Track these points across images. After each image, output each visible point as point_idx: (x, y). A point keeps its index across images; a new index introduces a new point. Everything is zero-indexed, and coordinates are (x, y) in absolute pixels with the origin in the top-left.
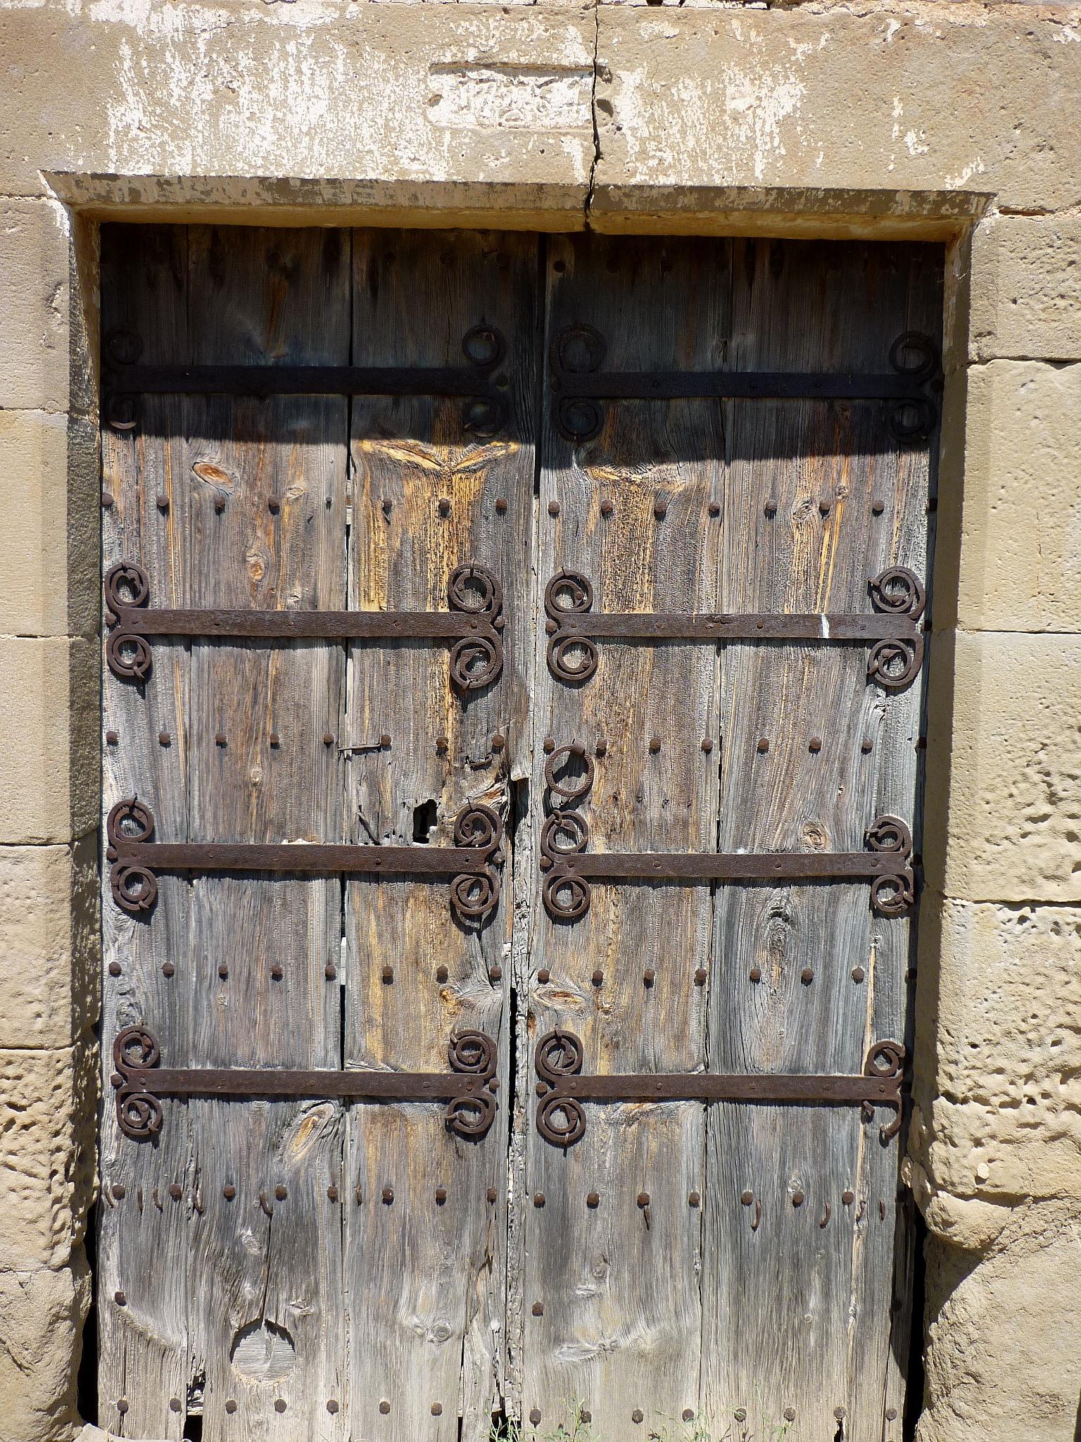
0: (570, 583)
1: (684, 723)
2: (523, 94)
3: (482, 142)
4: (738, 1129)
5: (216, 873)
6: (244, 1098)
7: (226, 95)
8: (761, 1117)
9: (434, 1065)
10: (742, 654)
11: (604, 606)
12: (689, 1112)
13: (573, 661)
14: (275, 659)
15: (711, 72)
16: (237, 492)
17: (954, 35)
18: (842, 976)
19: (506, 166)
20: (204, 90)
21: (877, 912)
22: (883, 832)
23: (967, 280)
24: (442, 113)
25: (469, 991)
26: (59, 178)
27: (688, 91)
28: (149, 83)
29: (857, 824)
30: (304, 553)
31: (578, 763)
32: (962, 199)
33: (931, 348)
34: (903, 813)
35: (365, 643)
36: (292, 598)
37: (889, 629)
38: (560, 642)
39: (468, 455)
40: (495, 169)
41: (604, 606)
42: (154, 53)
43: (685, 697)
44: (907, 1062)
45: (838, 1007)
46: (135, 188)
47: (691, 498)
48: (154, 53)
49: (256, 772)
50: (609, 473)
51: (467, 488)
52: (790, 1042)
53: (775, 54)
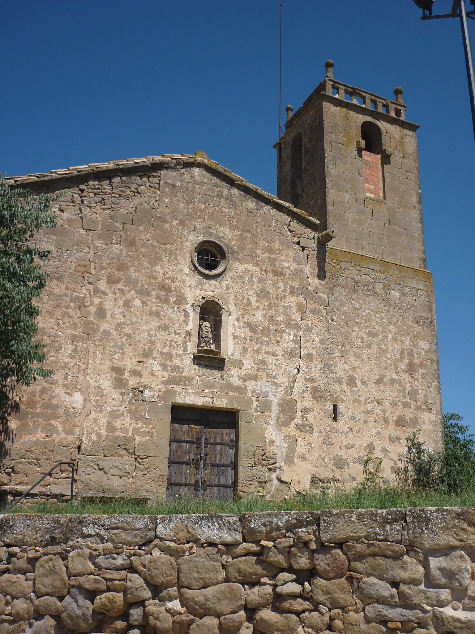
0: (206, 439)
1: (215, 452)
2: (207, 399)
3: (204, 402)
4: (220, 490)
5: (175, 463)
6: (177, 485)
7: (185, 397)
8: (222, 488)
9: (193, 483)
10: (220, 446)
11: (209, 441)
12: (216, 488)
13: (206, 446)
14: (181, 444)
15: (221, 398)
16: (179, 429)
17: (238, 397)
18: (228, 475)
19: (394, 525)
20: (183, 396)
21: (231, 469)
22: (232, 462)
23: (199, 329)
24: (201, 400)
25: (197, 476)
26: (172, 402)
27: (219, 400)
28: (179, 395)
29: (230, 461)
30: (184, 434)
31: (206, 455)
32: (239, 409)
33: (235, 420)
34: (233, 460)
35: (189, 443)
36: (183, 439)
37: (232, 444)
38: (205, 444)
39: (198, 427)
40: (205, 404)
41: (209, 441)
42: (180, 393)
43: (215, 449)
44: (234, 483)
45: (228, 478)
46: (177, 403)
47: (216, 432)
48: (180, 393)
49: (179, 454)
50: (209, 429)
51: (198, 430)
52: (224, 482)
53: (226, 397)
